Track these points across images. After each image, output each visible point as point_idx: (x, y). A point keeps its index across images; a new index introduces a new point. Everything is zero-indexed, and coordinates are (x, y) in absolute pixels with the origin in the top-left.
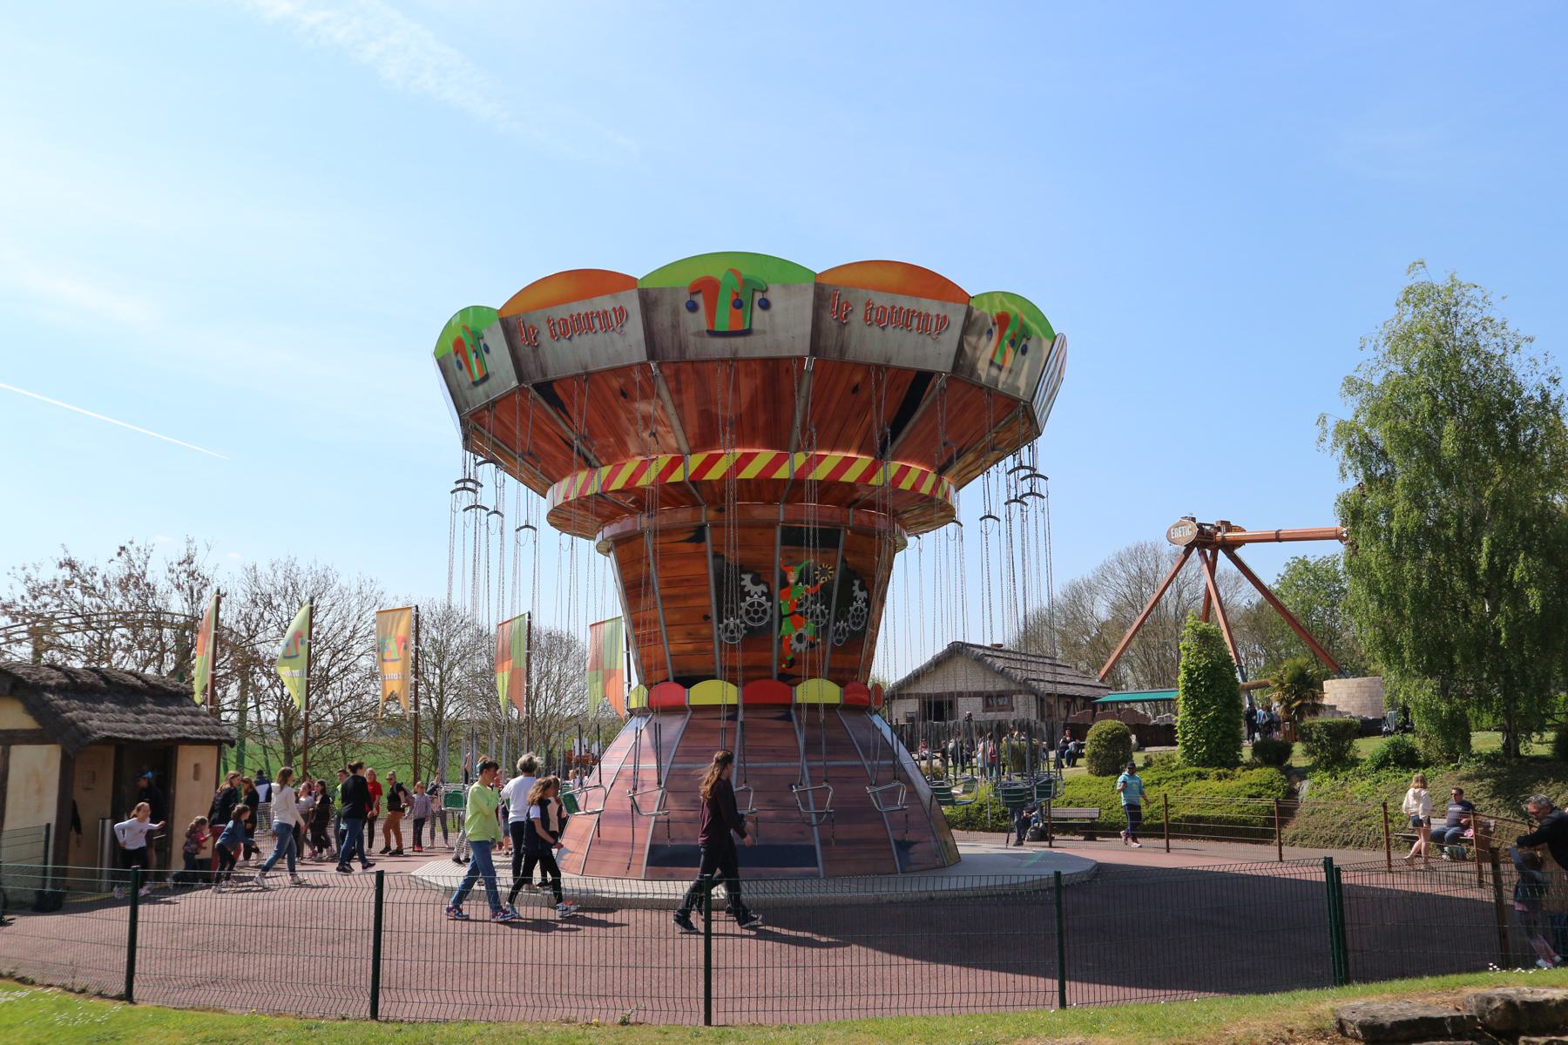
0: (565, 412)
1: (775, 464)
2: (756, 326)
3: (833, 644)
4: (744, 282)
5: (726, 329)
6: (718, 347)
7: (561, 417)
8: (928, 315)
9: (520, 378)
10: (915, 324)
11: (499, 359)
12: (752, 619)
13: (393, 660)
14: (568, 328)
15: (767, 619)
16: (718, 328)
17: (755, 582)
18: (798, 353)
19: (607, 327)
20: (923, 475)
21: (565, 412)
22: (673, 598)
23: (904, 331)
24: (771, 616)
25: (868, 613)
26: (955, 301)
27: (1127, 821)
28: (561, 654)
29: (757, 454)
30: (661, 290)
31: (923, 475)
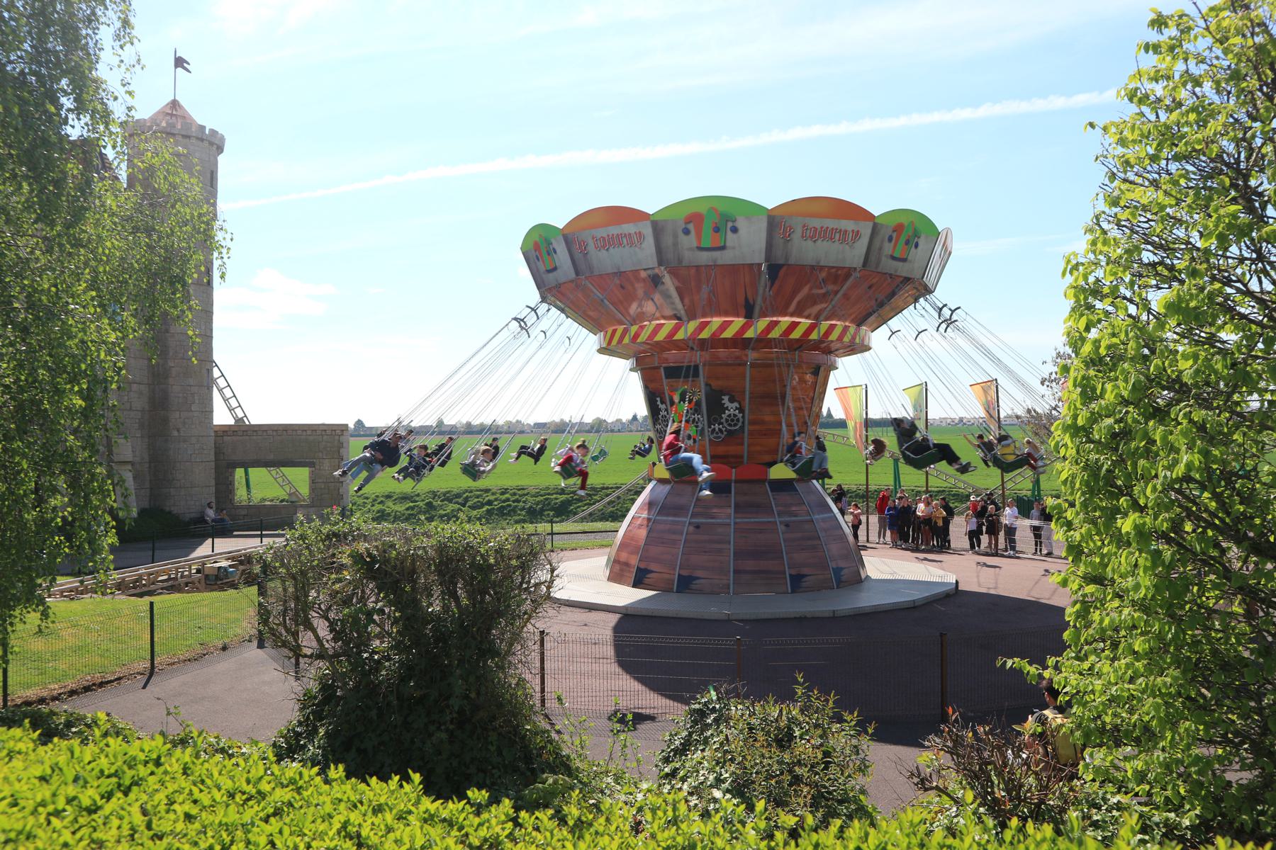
1: (744, 328)
3: (710, 440)
4: (720, 215)
6: (704, 258)
8: (846, 231)
9: (577, 273)
11: (562, 256)
12: (730, 425)
14: (607, 243)
15: (740, 424)
16: (704, 245)
17: (732, 401)
18: (757, 262)
19: (631, 244)
20: (846, 329)
23: (830, 242)
24: (743, 423)
25: (743, 417)
28: (42, 230)
30: (882, 225)
31: (846, 329)
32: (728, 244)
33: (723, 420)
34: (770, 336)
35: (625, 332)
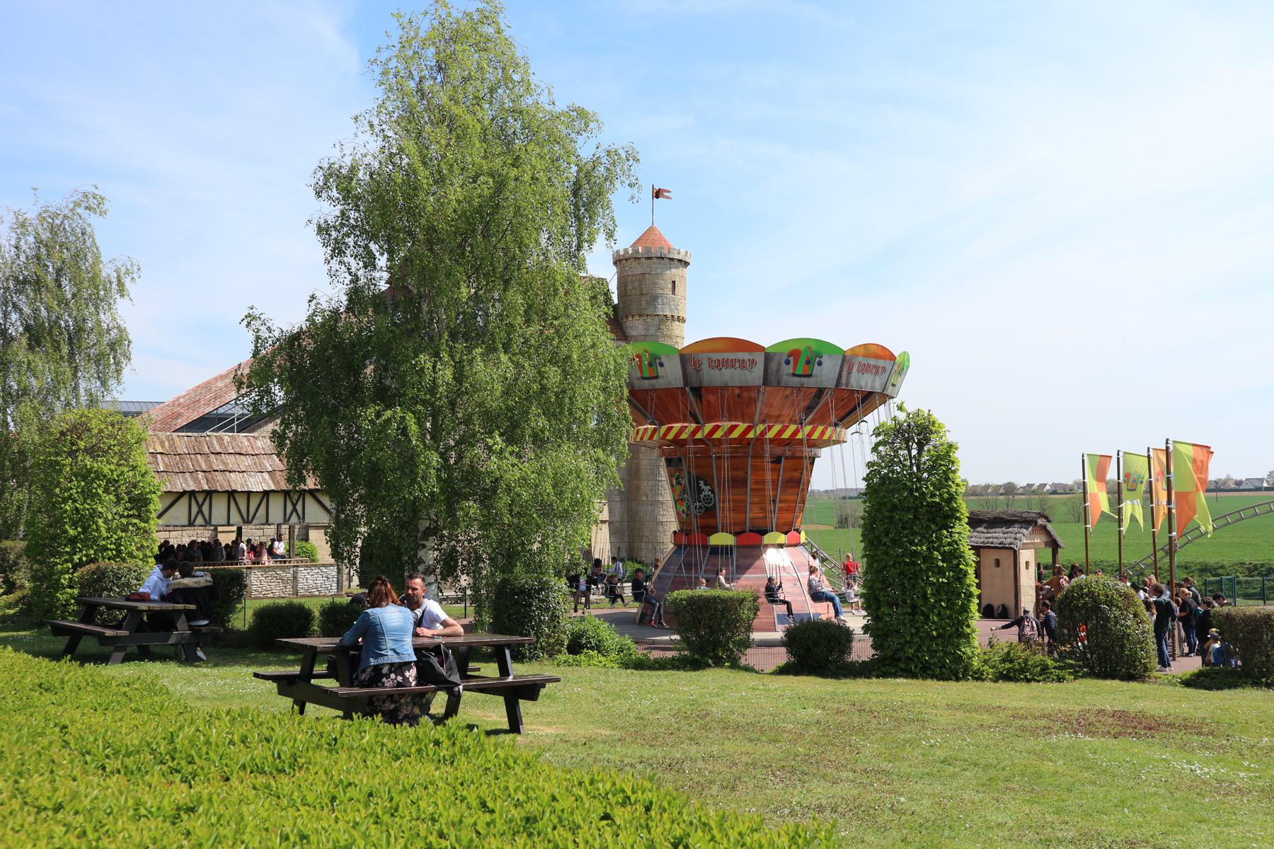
0: (701, 401)
1: (796, 432)
2: (660, 374)
5: (801, 373)
6: (796, 381)
7: (697, 404)
10: (737, 364)
13: (317, 527)
14: (720, 365)
17: (706, 484)
21: (701, 401)
22: (756, 490)
23: (732, 369)
26: (758, 351)
27: (414, 658)
29: (738, 426)
30: (775, 354)
32: (814, 373)
33: (701, 499)
34: (782, 437)
35: (655, 431)
